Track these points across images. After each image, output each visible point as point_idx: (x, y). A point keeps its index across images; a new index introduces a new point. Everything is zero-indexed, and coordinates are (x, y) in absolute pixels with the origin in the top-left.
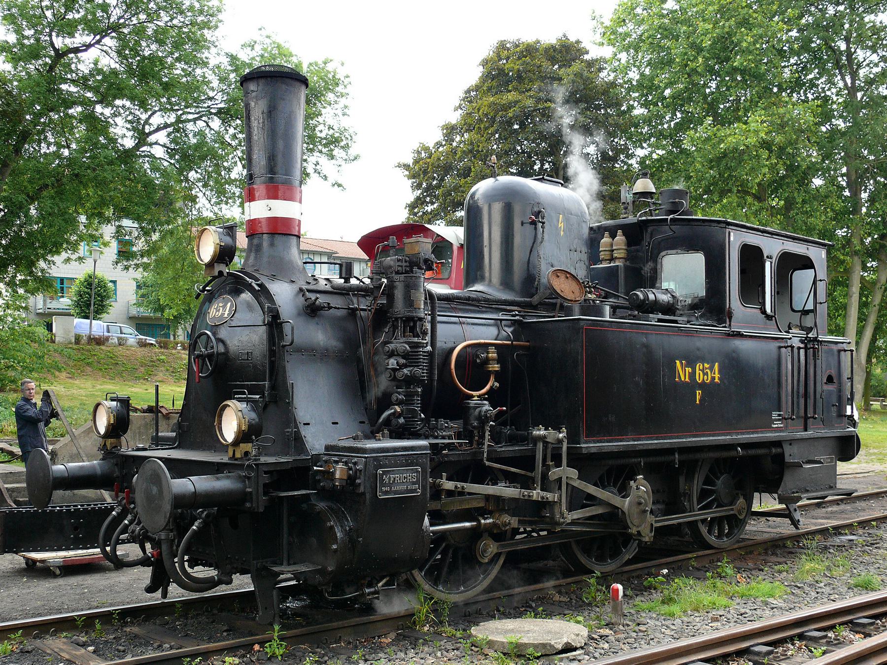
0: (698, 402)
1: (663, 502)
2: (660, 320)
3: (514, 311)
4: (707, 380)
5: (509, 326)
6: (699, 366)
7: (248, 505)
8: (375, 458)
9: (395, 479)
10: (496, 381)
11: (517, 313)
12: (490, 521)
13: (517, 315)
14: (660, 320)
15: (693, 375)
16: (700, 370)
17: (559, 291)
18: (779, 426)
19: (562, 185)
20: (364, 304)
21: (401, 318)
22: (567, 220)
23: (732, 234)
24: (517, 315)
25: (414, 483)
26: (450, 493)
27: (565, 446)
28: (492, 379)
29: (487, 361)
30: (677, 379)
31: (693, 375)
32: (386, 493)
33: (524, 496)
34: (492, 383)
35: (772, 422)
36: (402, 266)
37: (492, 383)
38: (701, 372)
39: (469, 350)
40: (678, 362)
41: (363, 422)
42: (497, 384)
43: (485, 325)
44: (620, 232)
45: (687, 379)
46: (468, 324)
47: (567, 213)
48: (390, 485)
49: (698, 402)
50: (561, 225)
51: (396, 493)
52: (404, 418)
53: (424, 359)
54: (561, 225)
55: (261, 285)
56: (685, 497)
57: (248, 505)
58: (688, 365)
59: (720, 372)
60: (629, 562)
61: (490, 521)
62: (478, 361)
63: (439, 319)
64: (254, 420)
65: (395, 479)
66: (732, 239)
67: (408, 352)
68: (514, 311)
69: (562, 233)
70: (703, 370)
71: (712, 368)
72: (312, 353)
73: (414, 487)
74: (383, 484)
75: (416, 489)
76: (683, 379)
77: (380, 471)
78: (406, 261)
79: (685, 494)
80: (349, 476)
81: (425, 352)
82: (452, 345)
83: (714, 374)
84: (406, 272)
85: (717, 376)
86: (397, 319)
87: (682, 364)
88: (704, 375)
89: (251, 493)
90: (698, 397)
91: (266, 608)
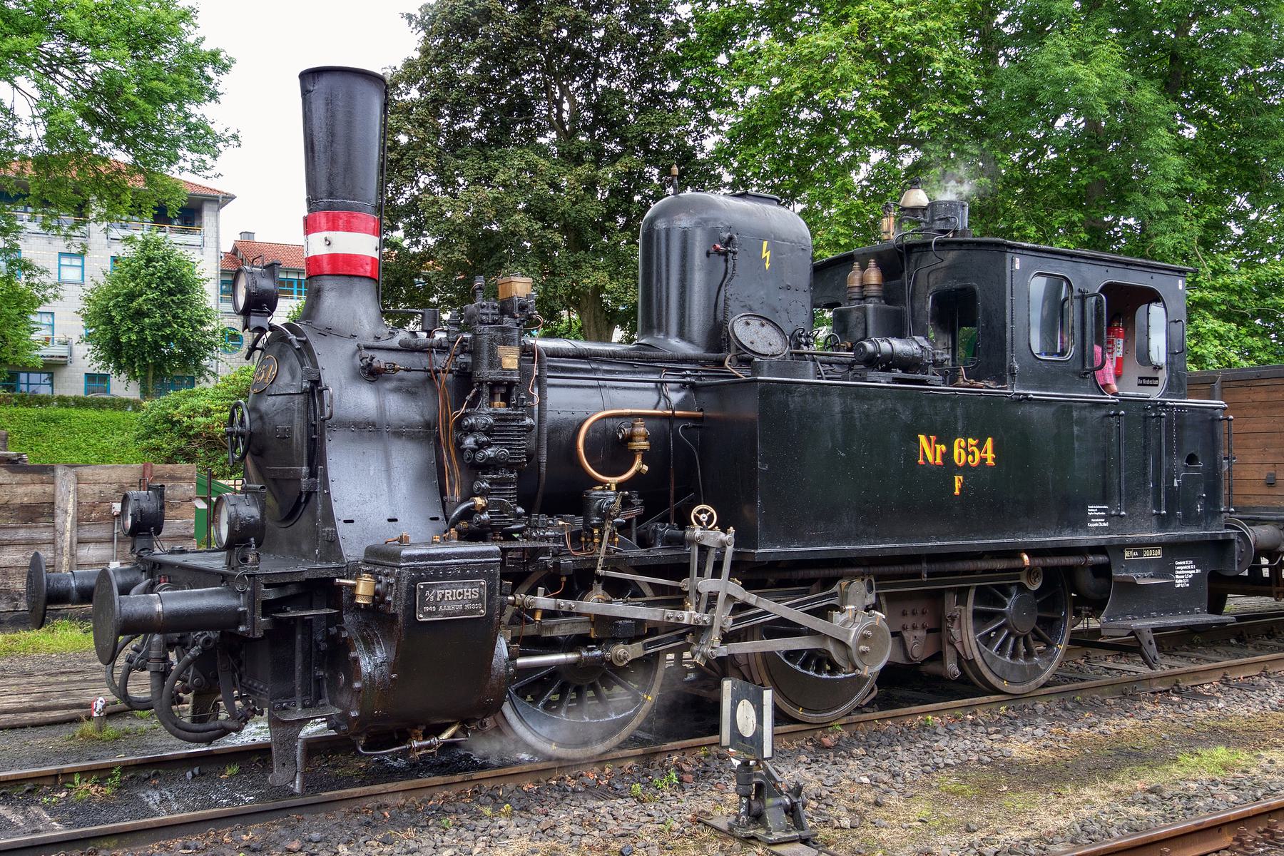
0: (957, 492)
1: (923, 627)
2: (896, 380)
3: (685, 370)
4: (974, 461)
5: (677, 391)
6: (958, 443)
7: (242, 628)
8: (415, 569)
9: (443, 595)
10: (644, 462)
11: (688, 372)
12: (598, 653)
13: (689, 376)
14: (896, 380)
15: (948, 456)
16: (960, 447)
17: (749, 346)
18: (1101, 525)
19: (779, 202)
20: (441, 360)
21: (486, 382)
22: (772, 247)
23: (1017, 260)
24: (689, 376)
25: (473, 601)
26: (547, 614)
27: (730, 549)
28: (638, 461)
29: (630, 438)
30: (921, 461)
31: (948, 456)
32: (430, 614)
33: (668, 618)
34: (638, 465)
35: (1089, 519)
36: (487, 314)
37: (638, 465)
38: (962, 451)
39: (609, 423)
40: (922, 438)
41: (437, 519)
42: (646, 468)
43: (638, 389)
44: (872, 263)
45: (938, 461)
46: (613, 388)
47: (777, 241)
48: (436, 604)
49: (957, 492)
50: (766, 254)
51: (446, 614)
52: (490, 513)
53: (519, 436)
54: (766, 254)
55: (305, 343)
56: (953, 620)
57: (242, 628)
58: (938, 442)
59: (994, 451)
60: (859, 709)
61: (598, 653)
62: (620, 437)
63: (550, 381)
64: (252, 517)
65: (443, 595)
66: (1017, 266)
67: (491, 425)
68: (685, 370)
69: (767, 265)
70: (966, 449)
71: (980, 446)
72: (368, 429)
73: (474, 606)
74: (424, 602)
75: (479, 610)
76: (930, 459)
77: (421, 585)
78: (494, 308)
79: (953, 618)
80: (377, 593)
81: (523, 426)
82: (584, 416)
83: (986, 452)
84: (494, 322)
85: (990, 456)
86: (481, 383)
87: (929, 440)
88: (968, 453)
89: (244, 612)
90: (957, 485)
91: (284, 764)
